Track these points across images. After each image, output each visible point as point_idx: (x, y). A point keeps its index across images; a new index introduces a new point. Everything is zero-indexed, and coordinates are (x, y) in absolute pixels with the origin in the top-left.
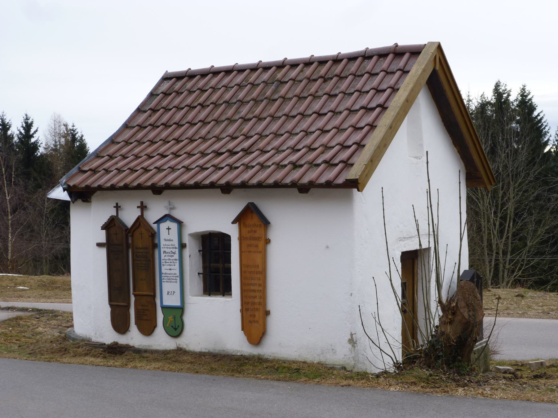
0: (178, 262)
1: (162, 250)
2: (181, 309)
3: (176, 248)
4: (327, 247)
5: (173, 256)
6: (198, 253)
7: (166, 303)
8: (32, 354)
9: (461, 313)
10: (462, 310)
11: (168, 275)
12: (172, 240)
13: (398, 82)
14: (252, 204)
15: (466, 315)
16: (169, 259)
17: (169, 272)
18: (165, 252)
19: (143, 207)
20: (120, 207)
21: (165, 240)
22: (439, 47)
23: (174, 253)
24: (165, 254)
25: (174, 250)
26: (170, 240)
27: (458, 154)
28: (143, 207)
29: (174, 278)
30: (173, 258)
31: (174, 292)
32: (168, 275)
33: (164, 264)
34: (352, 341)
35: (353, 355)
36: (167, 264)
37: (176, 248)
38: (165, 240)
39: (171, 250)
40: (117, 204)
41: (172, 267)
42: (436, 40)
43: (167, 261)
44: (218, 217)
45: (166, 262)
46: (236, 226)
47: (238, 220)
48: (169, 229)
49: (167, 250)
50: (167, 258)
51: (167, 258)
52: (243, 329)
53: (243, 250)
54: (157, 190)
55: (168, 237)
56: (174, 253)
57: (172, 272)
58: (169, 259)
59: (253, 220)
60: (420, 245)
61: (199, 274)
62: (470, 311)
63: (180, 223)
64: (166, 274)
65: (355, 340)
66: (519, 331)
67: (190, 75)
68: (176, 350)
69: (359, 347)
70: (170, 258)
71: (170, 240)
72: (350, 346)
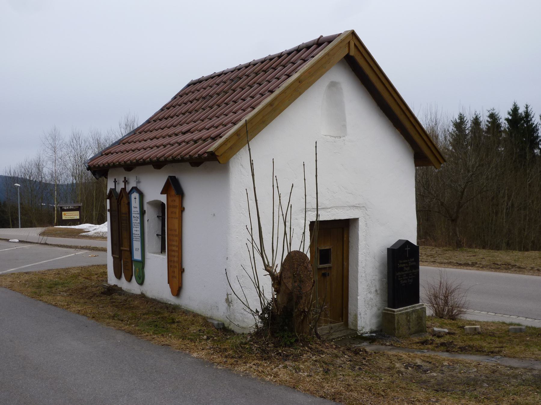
4: (214, 215)
6: (157, 219)
8: (482, 267)
9: (284, 283)
10: (285, 281)
15: (290, 285)
22: (353, 33)
27: (401, 136)
28: (126, 182)
34: (228, 302)
35: (229, 313)
40: (115, 179)
42: (350, 29)
46: (165, 196)
52: (169, 283)
60: (317, 215)
61: (157, 235)
62: (295, 282)
65: (230, 300)
66: (486, 291)
67: (200, 81)
68: (139, 295)
69: (235, 306)
72: (226, 305)
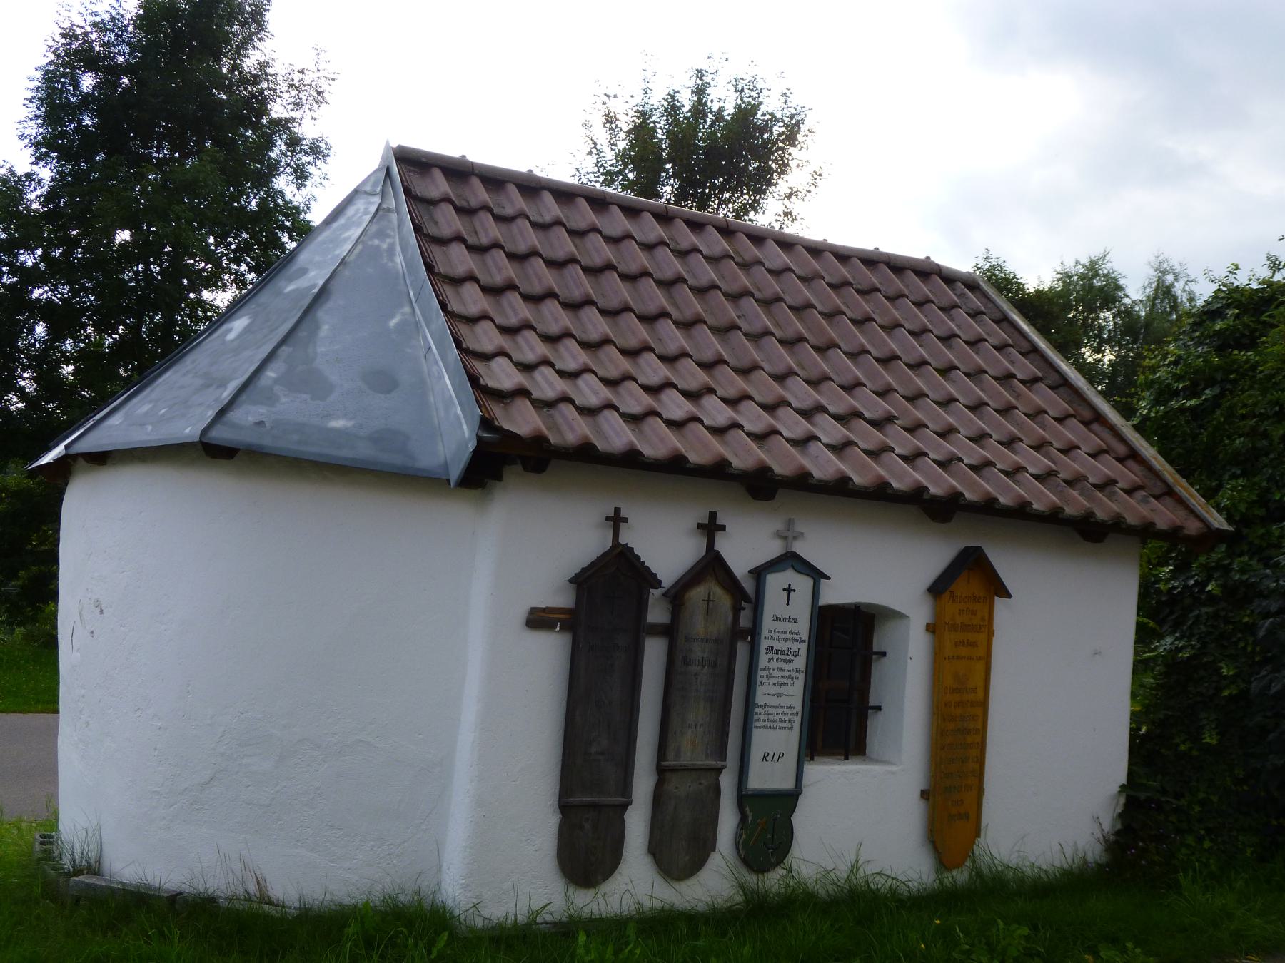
0: (802, 676)
1: (764, 644)
2: (788, 800)
3: (802, 641)
5: (790, 661)
7: (755, 782)
11: (771, 710)
12: (795, 621)
13: (363, 452)
14: (978, 550)
16: (780, 669)
17: (774, 701)
18: (770, 648)
19: (710, 528)
20: (626, 520)
21: (777, 619)
23: (796, 654)
24: (770, 656)
25: (795, 647)
26: (789, 620)
28: (710, 528)
29: (787, 718)
30: (790, 666)
31: (781, 755)
32: (771, 710)
33: (765, 680)
36: (772, 681)
37: (802, 641)
38: (777, 619)
39: (789, 644)
41: (784, 690)
43: (774, 674)
44: (885, 571)
45: (770, 677)
47: (937, 589)
48: (789, 590)
49: (777, 645)
50: (775, 665)
51: (775, 665)
53: (980, 666)
54: (761, 486)
55: (784, 612)
56: (796, 654)
57: (784, 701)
58: (780, 669)
59: (968, 587)
63: (817, 575)
64: (766, 706)
70: (783, 665)
71: (789, 620)
